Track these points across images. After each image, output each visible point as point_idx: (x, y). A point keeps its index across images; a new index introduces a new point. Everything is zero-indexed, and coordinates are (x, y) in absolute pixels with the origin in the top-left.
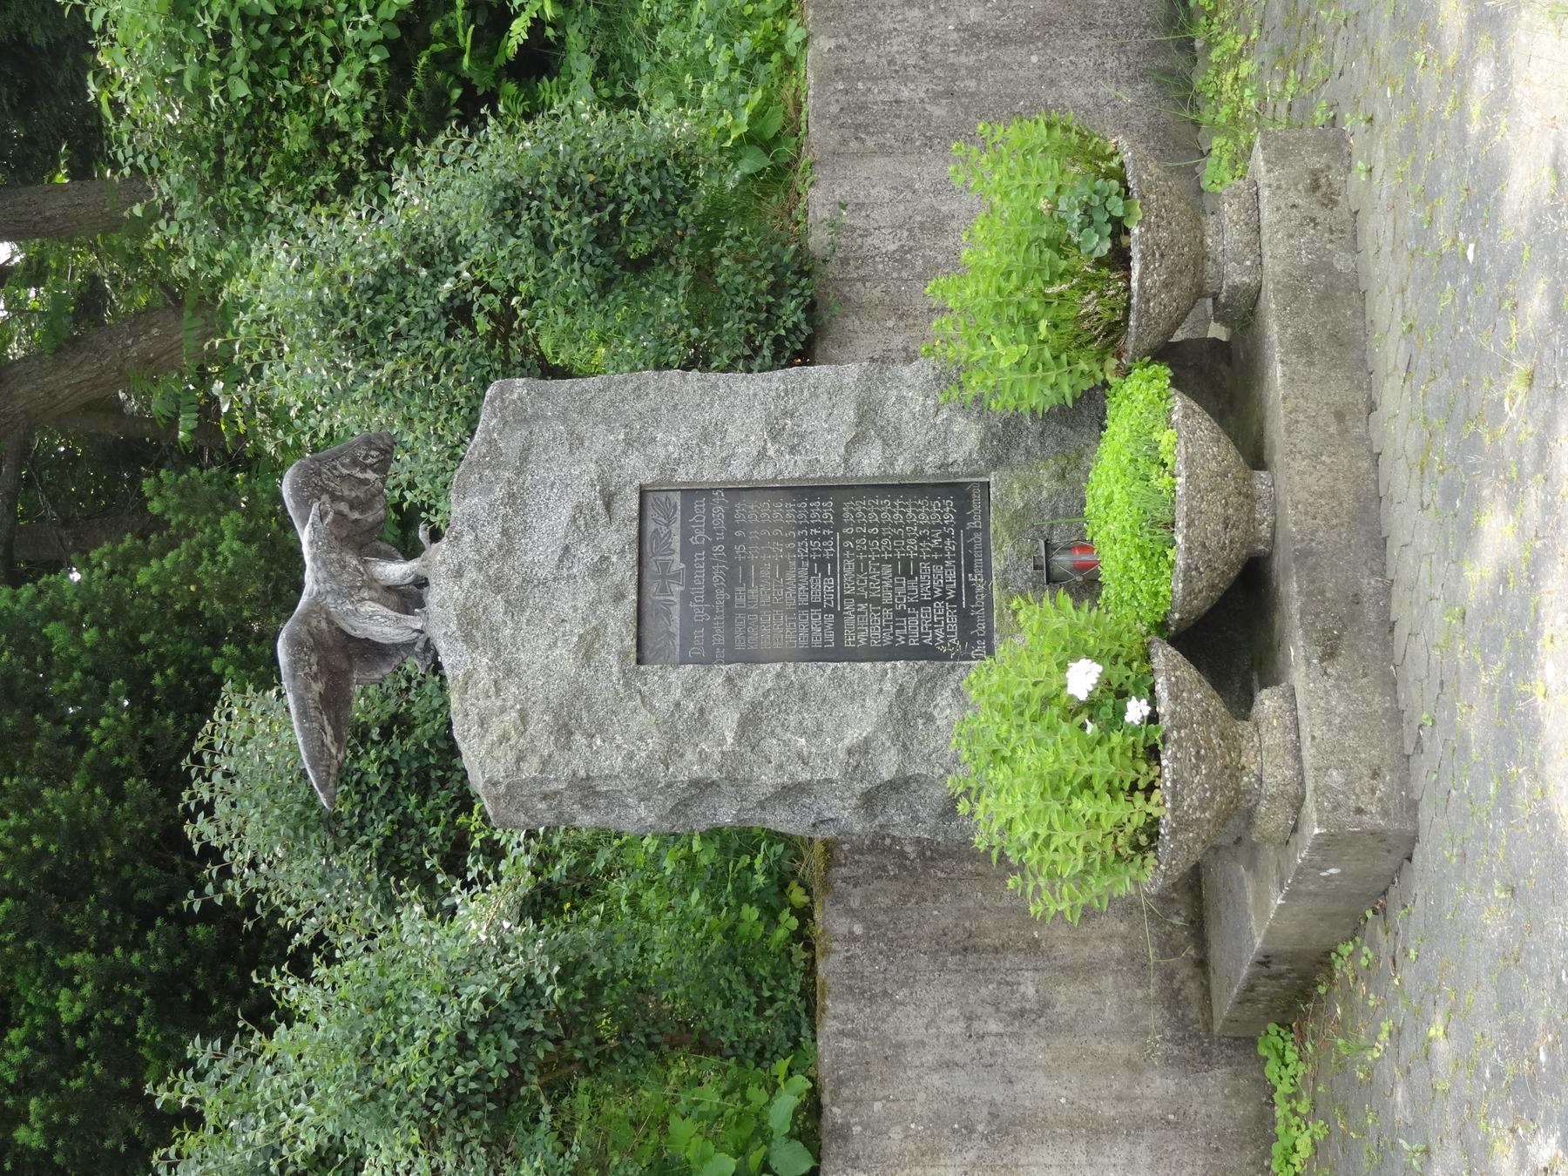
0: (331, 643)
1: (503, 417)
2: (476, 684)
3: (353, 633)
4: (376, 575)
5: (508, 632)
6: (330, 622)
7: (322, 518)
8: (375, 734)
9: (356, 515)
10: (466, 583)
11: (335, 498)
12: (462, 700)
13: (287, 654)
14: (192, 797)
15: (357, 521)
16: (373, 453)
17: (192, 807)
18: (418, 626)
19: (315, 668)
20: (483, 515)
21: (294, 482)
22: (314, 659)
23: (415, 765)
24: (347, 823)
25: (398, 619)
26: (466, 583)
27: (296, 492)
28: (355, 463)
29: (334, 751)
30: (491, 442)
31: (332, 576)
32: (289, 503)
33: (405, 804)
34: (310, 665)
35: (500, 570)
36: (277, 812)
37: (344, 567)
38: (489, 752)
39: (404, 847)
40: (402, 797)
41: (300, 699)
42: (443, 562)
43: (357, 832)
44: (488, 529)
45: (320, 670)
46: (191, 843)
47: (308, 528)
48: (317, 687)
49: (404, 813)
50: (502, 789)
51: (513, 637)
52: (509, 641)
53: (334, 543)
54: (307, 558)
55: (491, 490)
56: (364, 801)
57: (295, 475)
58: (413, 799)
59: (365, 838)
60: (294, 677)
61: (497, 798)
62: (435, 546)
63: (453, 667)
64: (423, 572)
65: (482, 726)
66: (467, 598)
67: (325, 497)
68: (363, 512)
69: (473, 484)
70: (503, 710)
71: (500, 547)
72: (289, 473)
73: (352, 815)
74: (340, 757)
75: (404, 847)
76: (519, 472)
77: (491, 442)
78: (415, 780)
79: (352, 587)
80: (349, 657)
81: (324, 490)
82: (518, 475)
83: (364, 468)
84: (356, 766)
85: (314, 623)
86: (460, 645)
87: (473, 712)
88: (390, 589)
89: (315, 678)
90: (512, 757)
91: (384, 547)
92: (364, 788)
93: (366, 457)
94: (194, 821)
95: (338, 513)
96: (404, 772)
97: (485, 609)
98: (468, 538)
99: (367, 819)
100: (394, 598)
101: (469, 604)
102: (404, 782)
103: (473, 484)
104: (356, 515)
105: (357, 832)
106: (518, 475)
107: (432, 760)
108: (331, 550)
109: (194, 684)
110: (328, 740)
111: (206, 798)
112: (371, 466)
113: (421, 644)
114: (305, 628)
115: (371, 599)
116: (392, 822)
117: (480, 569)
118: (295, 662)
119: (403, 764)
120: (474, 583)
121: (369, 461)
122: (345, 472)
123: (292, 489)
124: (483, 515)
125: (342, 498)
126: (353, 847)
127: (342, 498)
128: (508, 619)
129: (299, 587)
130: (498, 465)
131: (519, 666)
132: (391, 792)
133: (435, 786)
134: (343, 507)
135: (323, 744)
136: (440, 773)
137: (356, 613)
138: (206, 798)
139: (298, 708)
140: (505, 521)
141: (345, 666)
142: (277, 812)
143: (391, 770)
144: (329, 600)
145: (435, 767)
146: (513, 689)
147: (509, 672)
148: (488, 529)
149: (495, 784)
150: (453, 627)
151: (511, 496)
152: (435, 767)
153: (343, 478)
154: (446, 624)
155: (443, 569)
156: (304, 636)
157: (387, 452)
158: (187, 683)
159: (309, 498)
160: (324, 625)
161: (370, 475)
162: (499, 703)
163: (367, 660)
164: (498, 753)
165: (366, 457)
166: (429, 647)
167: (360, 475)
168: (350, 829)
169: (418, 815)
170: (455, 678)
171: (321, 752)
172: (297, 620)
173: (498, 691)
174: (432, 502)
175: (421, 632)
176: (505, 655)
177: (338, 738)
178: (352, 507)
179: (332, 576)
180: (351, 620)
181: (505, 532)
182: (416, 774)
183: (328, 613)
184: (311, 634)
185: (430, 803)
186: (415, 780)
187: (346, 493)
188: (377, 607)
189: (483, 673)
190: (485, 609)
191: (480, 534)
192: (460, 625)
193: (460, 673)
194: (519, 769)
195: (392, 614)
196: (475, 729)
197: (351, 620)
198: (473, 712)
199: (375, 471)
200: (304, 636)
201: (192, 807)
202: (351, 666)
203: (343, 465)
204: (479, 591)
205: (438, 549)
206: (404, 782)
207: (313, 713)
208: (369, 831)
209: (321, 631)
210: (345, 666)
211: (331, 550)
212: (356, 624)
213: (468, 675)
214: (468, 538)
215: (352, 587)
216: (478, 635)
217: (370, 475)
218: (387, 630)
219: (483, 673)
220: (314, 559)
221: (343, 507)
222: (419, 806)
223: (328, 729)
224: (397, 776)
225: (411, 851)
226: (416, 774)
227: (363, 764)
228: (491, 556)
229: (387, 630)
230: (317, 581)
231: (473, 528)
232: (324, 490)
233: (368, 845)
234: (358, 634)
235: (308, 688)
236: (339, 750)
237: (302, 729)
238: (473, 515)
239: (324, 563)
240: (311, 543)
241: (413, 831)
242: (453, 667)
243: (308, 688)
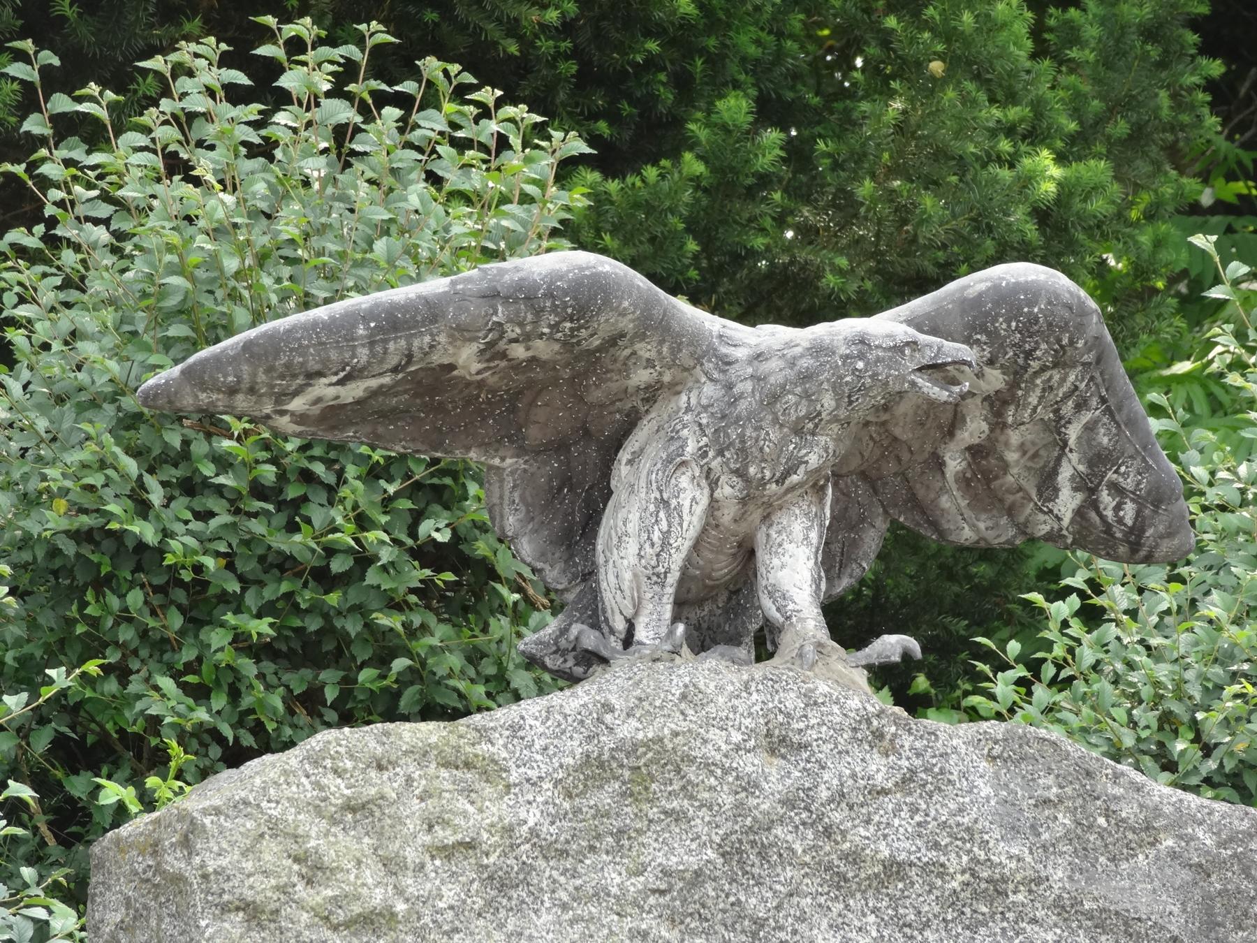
0: (596, 395)
1: (1222, 864)
2: (468, 791)
3: (624, 456)
4: (782, 518)
5: (613, 878)
6: (652, 394)
7: (933, 369)
8: (436, 530)
9: (954, 464)
10: (750, 764)
11: (998, 404)
12: (422, 754)
13: (555, 276)
14: (296, 46)
15: (940, 465)
16: (1129, 512)
17: (265, 50)
18: (641, 634)
19: (519, 352)
20: (942, 809)
21: (1032, 292)
22: (544, 349)
23: (353, 627)
24: (199, 447)
25: (659, 579)
26: (750, 764)
27: (1008, 299)
28: (1099, 460)
29: (297, 404)
30: (1148, 831)
31: (775, 398)
32: (975, 283)
33: (251, 600)
34: (526, 338)
35: (787, 857)
36: (231, 264)
37: (798, 431)
38: (275, 828)
39: (135, 598)
40: (269, 593)
41: (431, 311)
42: (811, 702)
43: (173, 474)
44: (904, 823)
45: (516, 366)
46: (164, 51)
47: (904, 332)
48: (468, 359)
49: (224, 598)
50: (174, 862)
51: (600, 894)
52: (589, 881)
53: (863, 404)
54: (821, 330)
55: (1013, 830)
56: (258, 490)
57: (1054, 298)
58: (262, 627)
59: (156, 496)
60: (492, 296)
61: (155, 848)
62: (861, 677)
63: (515, 729)
64: (788, 643)
65: (349, 807)
66: (708, 766)
67: (995, 380)
68: (965, 482)
69: (1030, 782)
70: (392, 865)
71: (854, 857)
72: (1057, 280)
73: (223, 462)
74: (284, 422)
75: (135, 598)
76: (1066, 909)
77: (1148, 831)
78: (313, 624)
79: (743, 451)
80: (560, 447)
81: (1017, 376)
82: (1058, 906)
83: (1087, 486)
84: (351, 471)
85: (645, 350)
86: (574, 748)
87: (386, 785)
88: (747, 554)
89: (491, 352)
90: (260, 889)
91: (872, 540)
92: (292, 492)
93: (1116, 489)
94: (225, 61)
95: (953, 420)
96: (333, 599)
97: (677, 816)
98: (878, 768)
99: (213, 503)
100: (723, 568)
101: (691, 773)
102: (305, 598)
103: (1030, 782)
104: (954, 464)
105: (173, 474)
106: (1058, 906)
107: (366, 676)
108: (847, 396)
109: (652, 63)
110: (324, 389)
111: (289, 81)
112: (1092, 503)
113: (590, 640)
114: (627, 324)
115: (714, 505)
116: (198, 568)
117: (790, 803)
118: (530, 299)
119: (354, 596)
120: (750, 786)
121: (1107, 499)
122: (1073, 433)
123: (1017, 288)
124: (942, 809)
125: (998, 424)
126: (131, 466)
127: (998, 424)
128: (650, 879)
129: (749, 316)
130: (1084, 851)
131: (519, 909)
132: (284, 564)
133: (298, 681)
134: (975, 428)
135: (312, 376)
136: (331, 694)
137: (676, 463)
138: (289, 81)
139: (407, 307)
140: (925, 868)
141: (534, 434)
142: (231, 264)
143: (339, 565)
144: (710, 391)
145: (348, 683)
146: (451, 894)
147: (500, 882)
148: (904, 823)
149: (186, 843)
150: (627, 729)
151: (998, 888)
152: (348, 683)
153: (1057, 425)
154: (640, 707)
155: (792, 701)
156: (605, 325)
157: (1135, 547)
158: (653, 46)
159: (993, 335)
160: (641, 377)
161: (1067, 502)
162: (411, 855)
163: (554, 495)
164: (271, 851)
165: (1116, 489)
166: (593, 660)
167: (1065, 473)
168: (185, 454)
169: (217, 638)
170: (483, 734)
171: (290, 372)
172: (649, 304)
173: (446, 852)
174: (1049, 671)
175: (628, 640)
176: (547, 870)
177: (333, 415)
178: (976, 452)
179: (775, 398)
180: (656, 452)
181: (894, 869)
182: (328, 630)
183: (675, 388)
184: (613, 341)
185: (248, 667)
186: (313, 624)
187: (1014, 437)
188: (692, 522)
189: (498, 810)
190: (677, 816)
191: (889, 803)
192: (633, 749)
193: (498, 749)
194: (225, 909)
195: (676, 560)
196: (339, 789)
197: (656, 452)
198: (386, 785)
199: (1079, 513)
200: (605, 325)
201: (265, 50)
202: (537, 452)
203: (1090, 428)
204: (728, 800)
205: (848, 686)
206: (305, 598)
207: (396, 348)
208: (181, 506)
209: (625, 370)
210: (534, 434)
211: (847, 396)
212: (645, 464)
213: (491, 771)
214: (878, 768)
215: (743, 451)
216: (604, 797)
217: (1067, 502)
218: (632, 547)
219: (498, 810)
220: (818, 350)
221: (975, 428)
222: (241, 642)
223: (354, 391)
224: (324, 578)
225: (125, 617)
226: (328, 630)
227: (355, 489)
228: (828, 832)
229: (632, 547)
230: (759, 357)
231: (906, 782)
232: (1017, 376)
233: (143, 508)
234: (622, 471)
235: (462, 333)
236: (300, 419)
237: (352, 318)
238: (939, 782)
239: (806, 377)
240: (862, 341)
241: (176, 621)
242: (515, 729)
243: (462, 333)
